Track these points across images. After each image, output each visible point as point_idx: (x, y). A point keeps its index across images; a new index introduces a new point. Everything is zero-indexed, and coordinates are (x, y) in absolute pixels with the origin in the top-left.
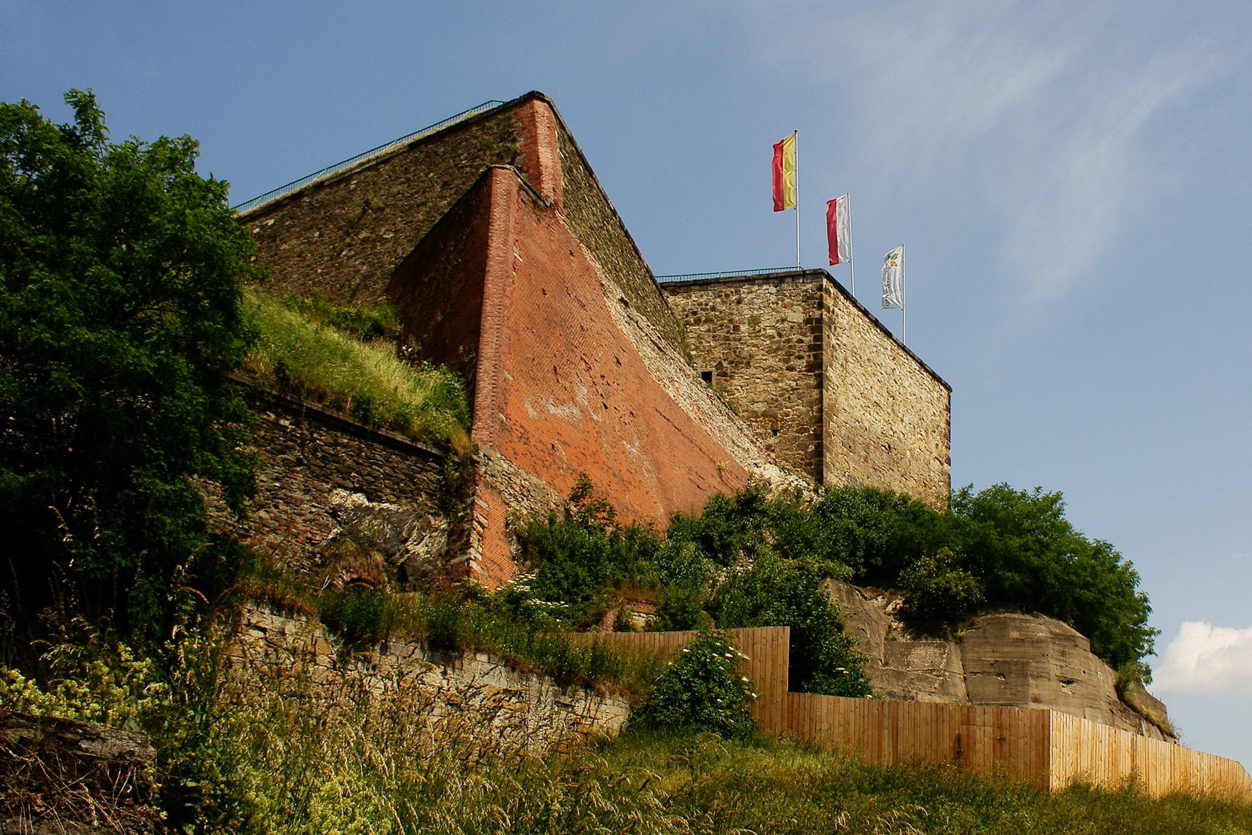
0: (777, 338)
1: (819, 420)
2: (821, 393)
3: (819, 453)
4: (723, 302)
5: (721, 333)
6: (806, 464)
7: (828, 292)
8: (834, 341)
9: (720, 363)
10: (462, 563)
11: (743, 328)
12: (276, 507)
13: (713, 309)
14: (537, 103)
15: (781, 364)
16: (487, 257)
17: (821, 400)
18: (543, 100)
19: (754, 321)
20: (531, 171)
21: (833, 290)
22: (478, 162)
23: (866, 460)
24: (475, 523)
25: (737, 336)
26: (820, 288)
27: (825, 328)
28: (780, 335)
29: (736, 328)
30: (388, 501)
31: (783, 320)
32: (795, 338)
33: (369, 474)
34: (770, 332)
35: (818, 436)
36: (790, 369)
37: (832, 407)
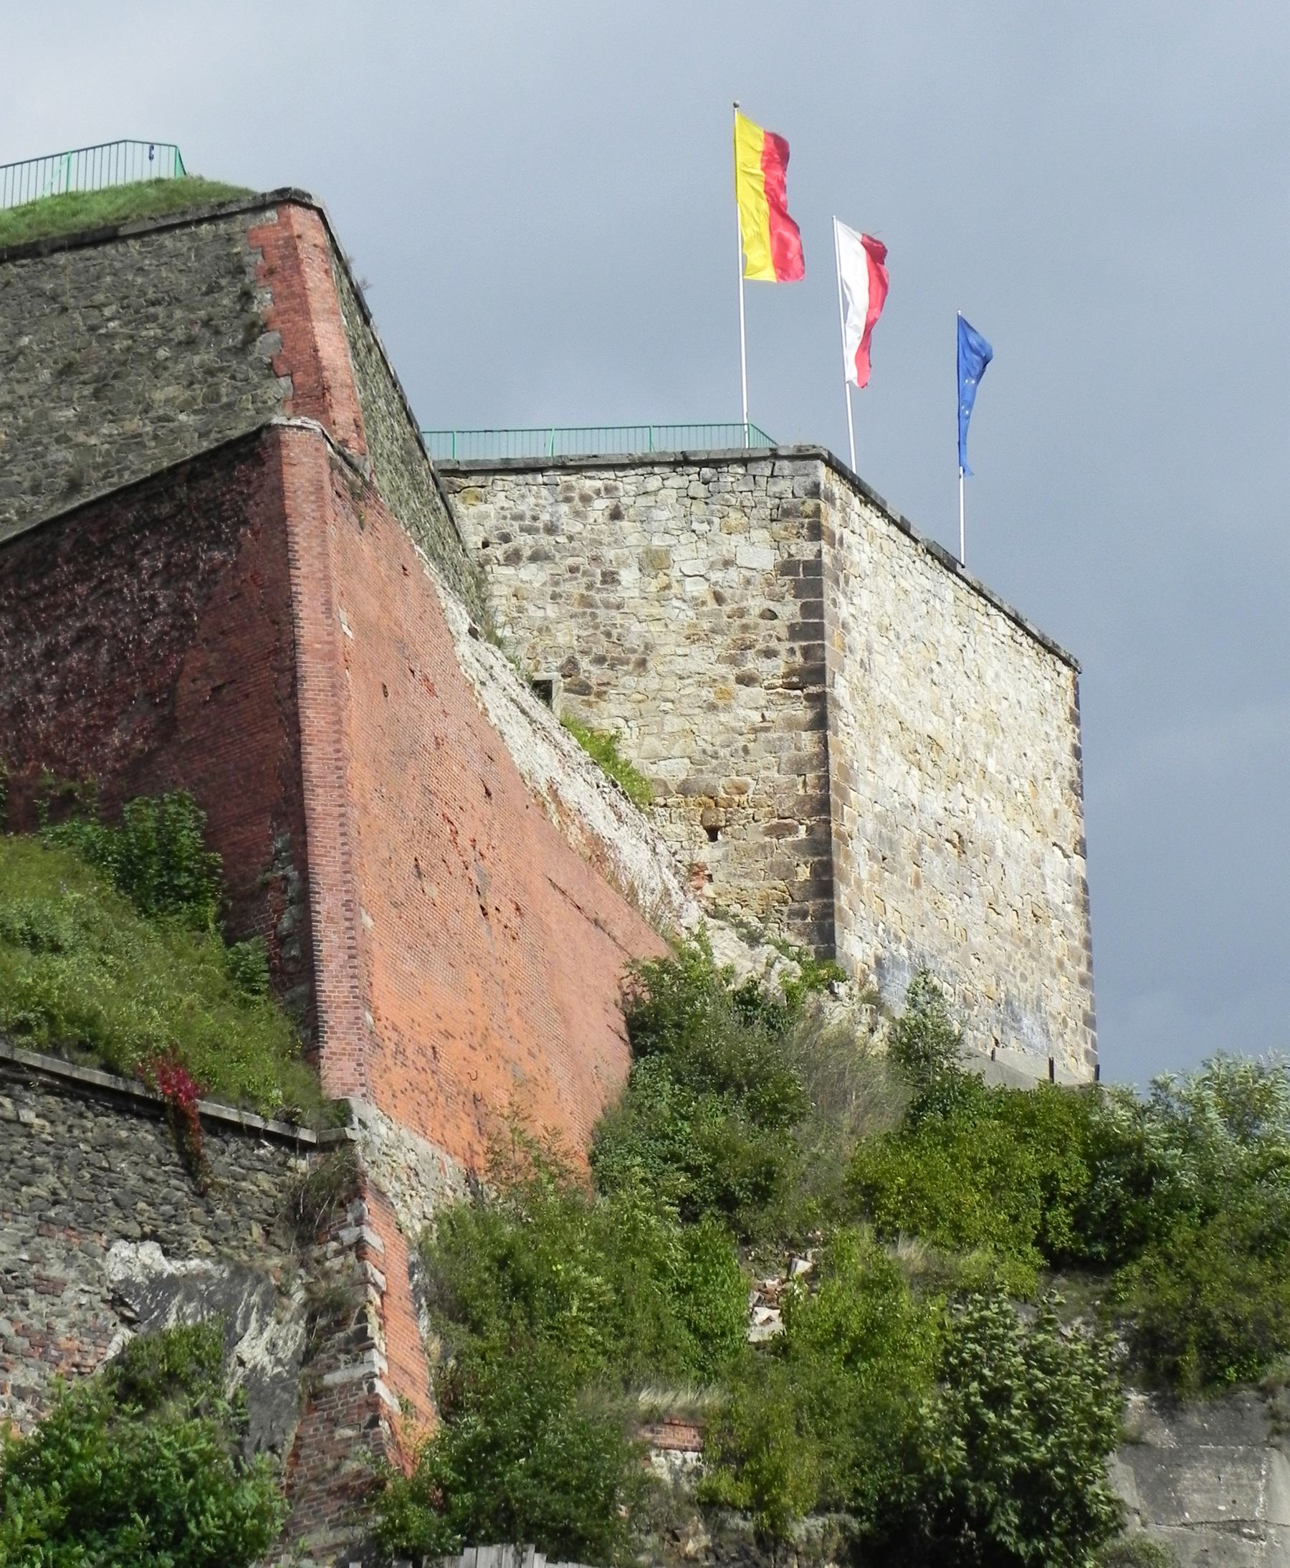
0: (712, 604)
1: (823, 806)
2: (824, 742)
3: (823, 885)
4: (577, 514)
5: (574, 588)
6: (792, 914)
7: (830, 499)
8: (845, 611)
9: (572, 662)
10: (354, 1385)
11: (628, 576)
12: (24, 1305)
13: (551, 529)
14: (295, 212)
15: (723, 669)
16: (294, 644)
17: (823, 759)
18: (309, 207)
19: (654, 562)
20: (299, 377)
21: (840, 490)
22: (152, 331)
23: (917, 883)
24: (371, 1290)
25: (613, 598)
26: (814, 491)
27: (827, 583)
28: (719, 599)
29: (610, 578)
30: (199, 1254)
31: (727, 564)
32: (756, 604)
33: (166, 1200)
34: (697, 588)
35: (822, 850)
36: (746, 680)
37: (846, 771)
